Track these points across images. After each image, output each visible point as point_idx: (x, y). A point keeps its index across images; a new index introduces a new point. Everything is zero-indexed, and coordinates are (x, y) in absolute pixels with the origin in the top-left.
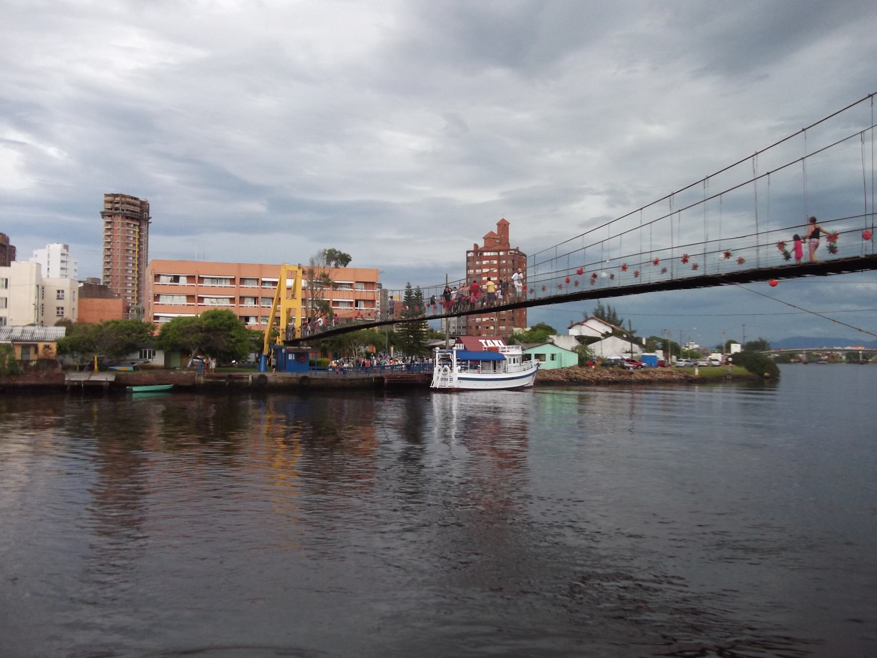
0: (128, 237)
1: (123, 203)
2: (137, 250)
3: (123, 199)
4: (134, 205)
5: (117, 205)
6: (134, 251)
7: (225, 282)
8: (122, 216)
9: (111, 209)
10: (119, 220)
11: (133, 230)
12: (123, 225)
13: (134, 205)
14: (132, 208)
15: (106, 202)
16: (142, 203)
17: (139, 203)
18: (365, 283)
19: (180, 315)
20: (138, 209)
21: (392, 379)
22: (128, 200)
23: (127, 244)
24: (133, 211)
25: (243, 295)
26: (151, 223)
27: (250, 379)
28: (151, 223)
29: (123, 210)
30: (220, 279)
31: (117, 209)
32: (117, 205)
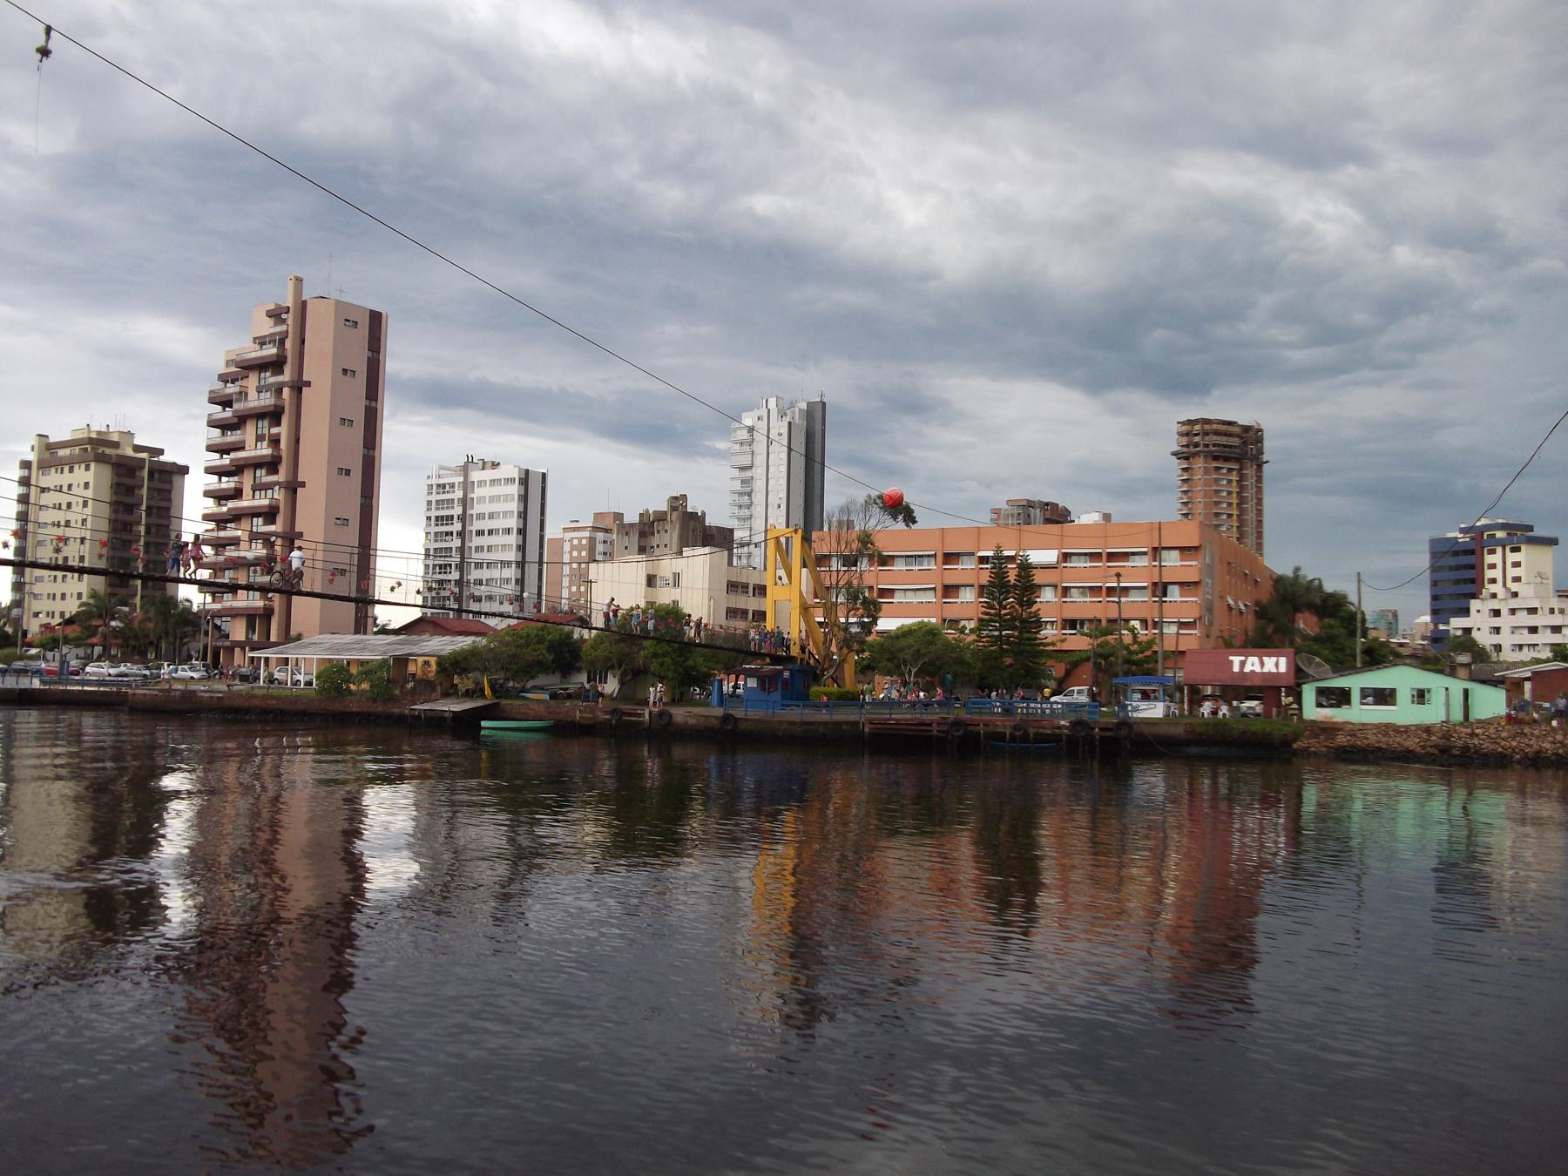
0: (1217, 492)
1: (1206, 434)
2: (1235, 513)
3: (1207, 427)
4: (1226, 434)
5: (1197, 439)
6: (1230, 516)
7: (929, 562)
8: (1205, 457)
9: (1187, 446)
10: (1199, 463)
11: (1227, 481)
12: (1206, 471)
13: (1226, 434)
14: (1223, 440)
15: (1181, 434)
16: (1246, 429)
17: (1235, 430)
18: (1182, 549)
19: (920, 619)
20: (1235, 441)
21: (879, 726)
22: (1214, 426)
23: (1217, 503)
24: (1225, 446)
25: (947, 582)
26: (1267, 462)
27: (647, 716)
28: (1267, 462)
29: (1207, 446)
30: (920, 556)
31: (1197, 445)
32: (1197, 439)
